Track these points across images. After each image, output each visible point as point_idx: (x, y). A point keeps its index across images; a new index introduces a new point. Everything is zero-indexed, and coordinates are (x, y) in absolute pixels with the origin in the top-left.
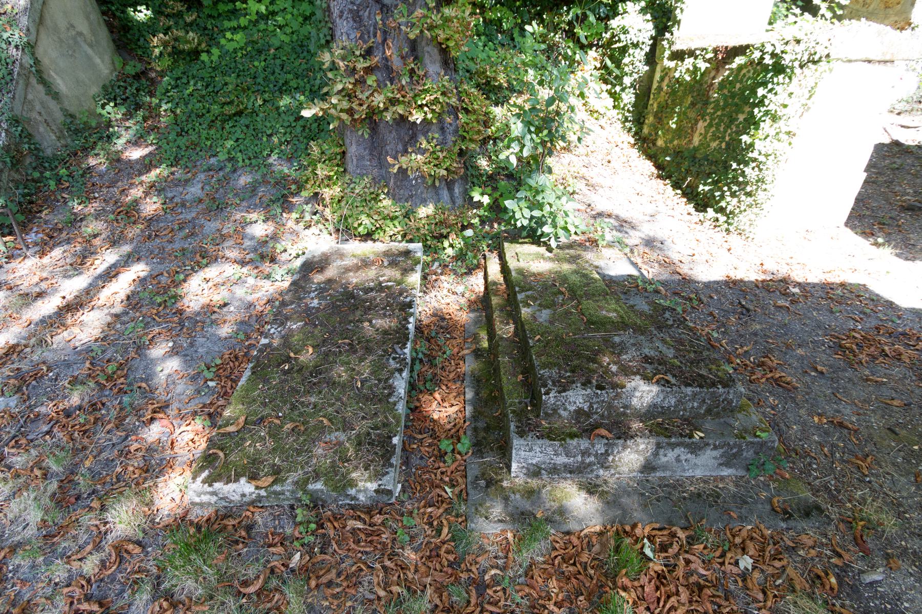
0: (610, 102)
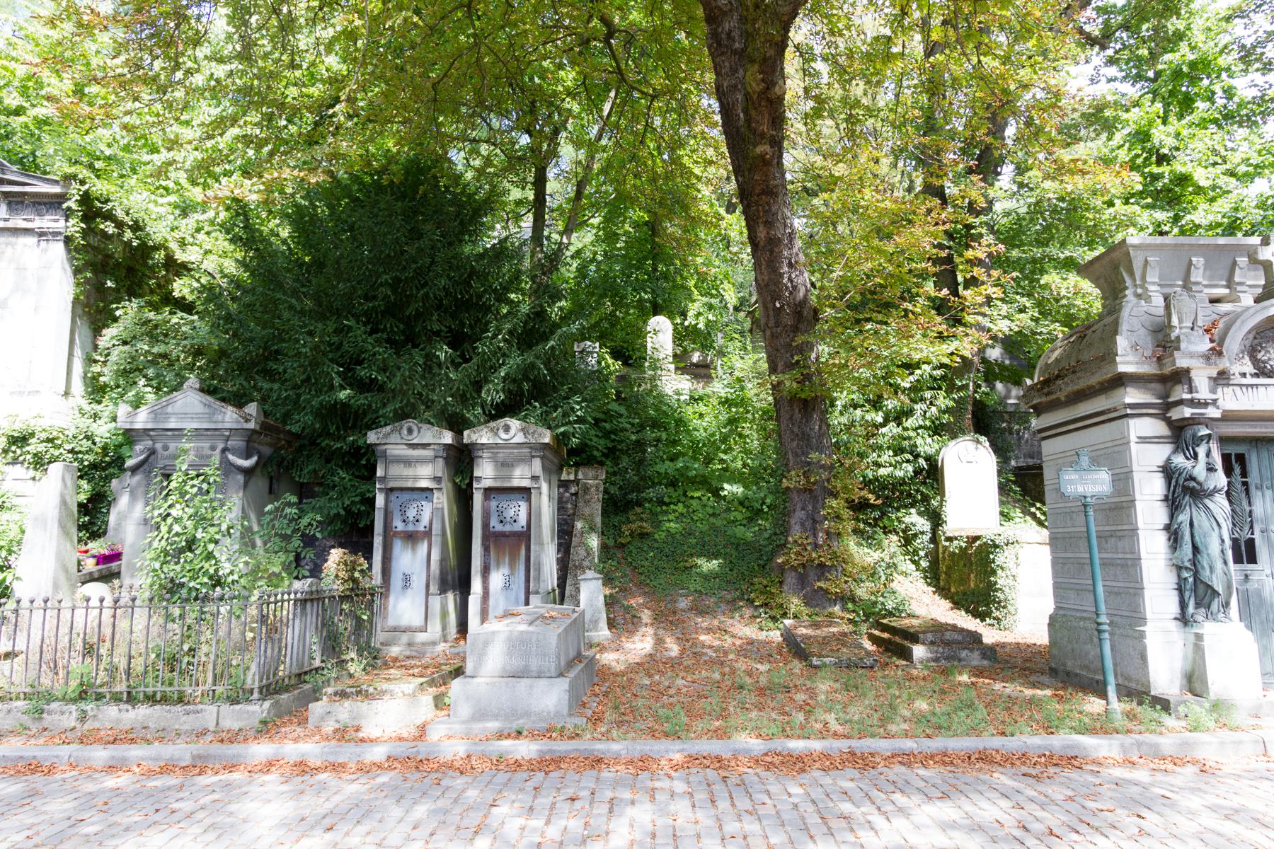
0: (913, 567)
